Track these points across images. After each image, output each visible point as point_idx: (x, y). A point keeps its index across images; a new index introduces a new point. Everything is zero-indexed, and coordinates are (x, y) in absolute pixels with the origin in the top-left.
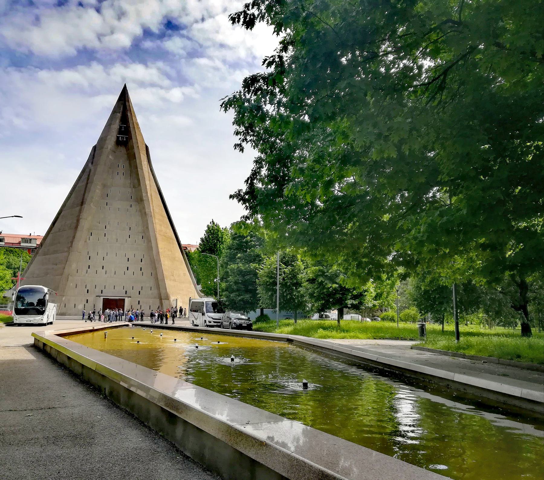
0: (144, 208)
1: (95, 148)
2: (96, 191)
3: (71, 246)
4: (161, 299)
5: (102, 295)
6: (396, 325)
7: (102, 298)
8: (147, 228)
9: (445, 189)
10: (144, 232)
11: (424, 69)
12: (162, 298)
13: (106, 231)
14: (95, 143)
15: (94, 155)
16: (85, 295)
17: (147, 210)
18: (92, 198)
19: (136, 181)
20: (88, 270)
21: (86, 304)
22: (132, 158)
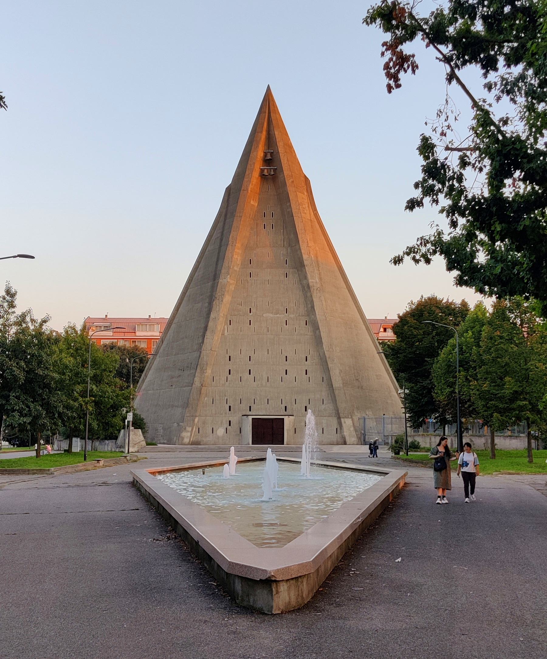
0: (306, 278)
1: (229, 190)
2: (235, 256)
3: (203, 342)
4: (339, 418)
5: (250, 413)
6: (497, 440)
7: (250, 418)
8: (313, 307)
9: (470, 218)
10: (308, 315)
11: (459, 17)
12: (341, 415)
13: (251, 316)
14: (228, 181)
15: (228, 200)
16: (226, 413)
17: (310, 281)
18: (229, 267)
19: (292, 236)
20: (229, 376)
21: (229, 427)
22: (283, 200)
